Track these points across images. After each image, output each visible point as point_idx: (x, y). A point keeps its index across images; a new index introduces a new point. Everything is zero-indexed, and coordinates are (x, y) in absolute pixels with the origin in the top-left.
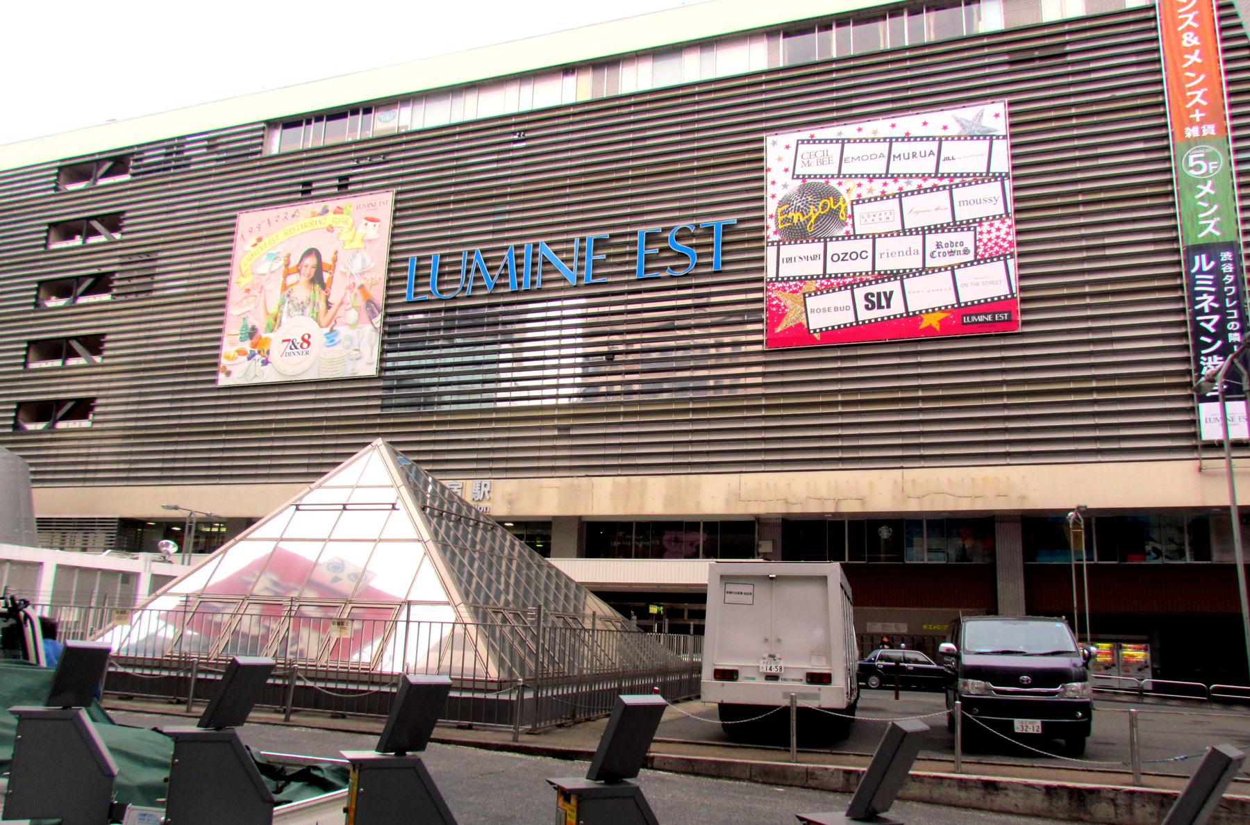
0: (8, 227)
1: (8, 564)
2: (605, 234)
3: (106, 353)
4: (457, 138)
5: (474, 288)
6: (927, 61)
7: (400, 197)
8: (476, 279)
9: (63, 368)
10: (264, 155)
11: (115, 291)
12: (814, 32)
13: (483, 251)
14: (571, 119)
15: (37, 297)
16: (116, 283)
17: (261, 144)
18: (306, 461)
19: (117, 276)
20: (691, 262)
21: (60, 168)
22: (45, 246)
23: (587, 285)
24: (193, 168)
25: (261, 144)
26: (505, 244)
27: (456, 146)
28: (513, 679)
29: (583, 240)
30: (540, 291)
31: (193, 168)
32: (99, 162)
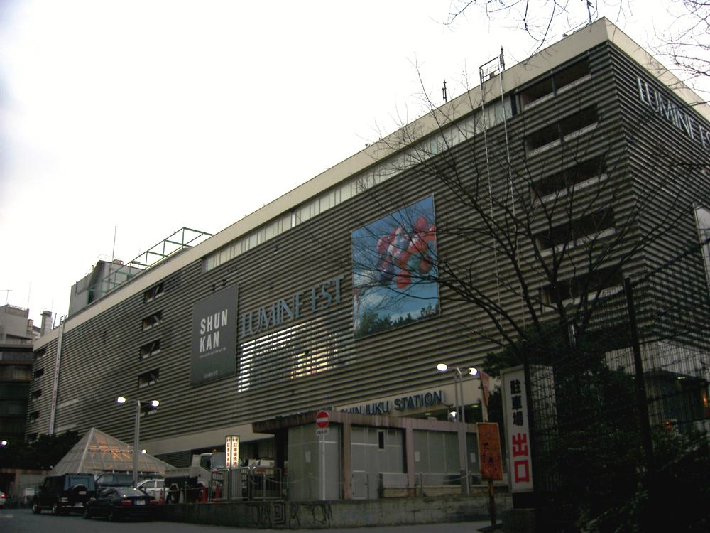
0: (291, 250)
1: (444, 435)
2: (302, 292)
3: (160, 377)
4: (594, 88)
5: (285, 319)
6: (625, 67)
7: (437, 198)
8: (284, 315)
9: (149, 386)
10: (202, 273)
11: (162, 347)
12: (504, 95)
13: (286, 300)
14: (292, 236)
15: (140, 354)
16: (162, 344)
17: (200, 269)
18: (401, 380)
19: (162, 340)
20: (329, 301)
21: (145, 293)
22: (142, 330)
23: (299, 318)
24: (182, 284)
25: (200, 269)
26: (270, 304)
27: (595, 94)
28: (486, 512)
29: (276, 304)
30: (283, 324)
31: (182, 284)
32: (155, 287)
